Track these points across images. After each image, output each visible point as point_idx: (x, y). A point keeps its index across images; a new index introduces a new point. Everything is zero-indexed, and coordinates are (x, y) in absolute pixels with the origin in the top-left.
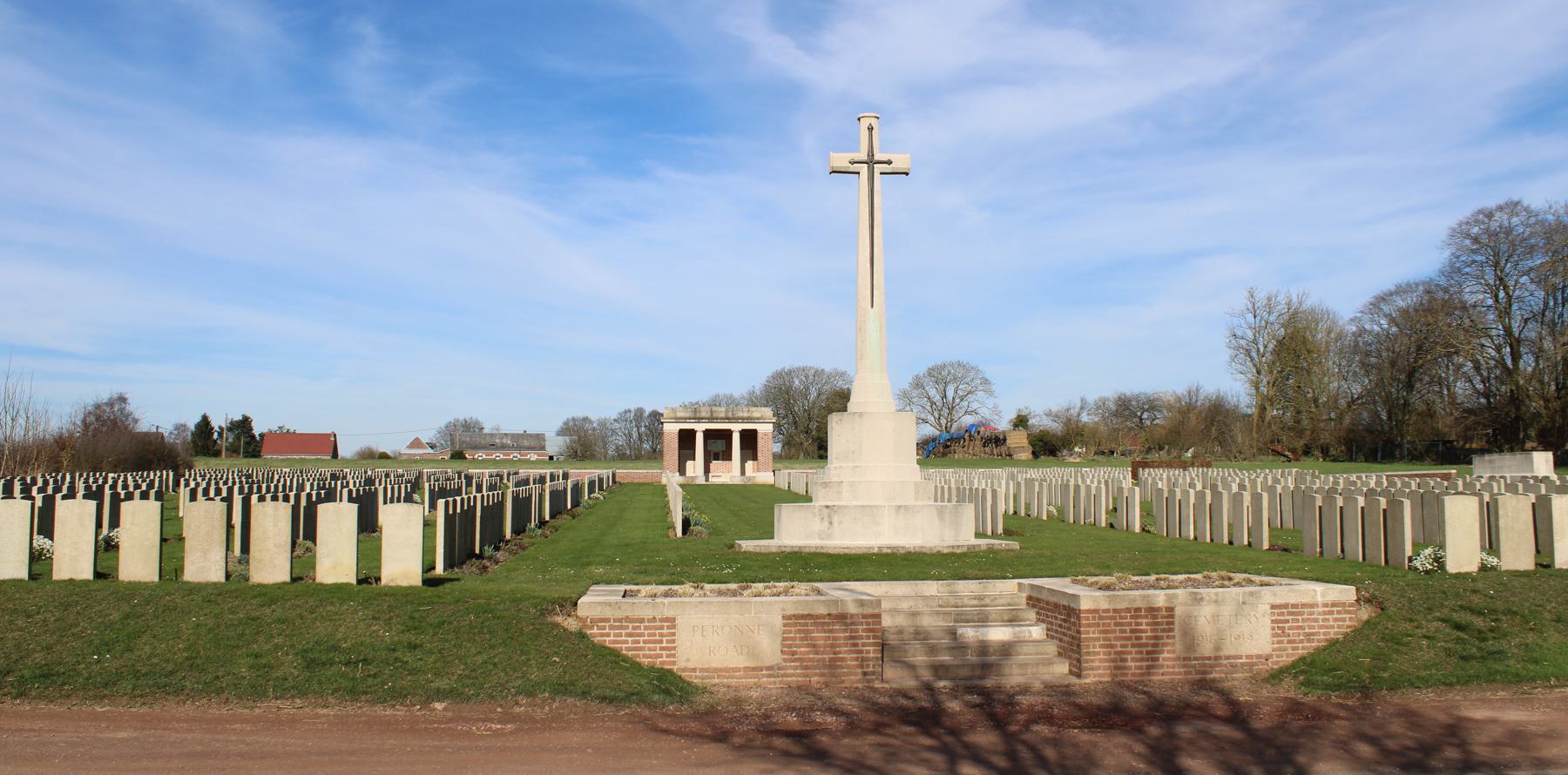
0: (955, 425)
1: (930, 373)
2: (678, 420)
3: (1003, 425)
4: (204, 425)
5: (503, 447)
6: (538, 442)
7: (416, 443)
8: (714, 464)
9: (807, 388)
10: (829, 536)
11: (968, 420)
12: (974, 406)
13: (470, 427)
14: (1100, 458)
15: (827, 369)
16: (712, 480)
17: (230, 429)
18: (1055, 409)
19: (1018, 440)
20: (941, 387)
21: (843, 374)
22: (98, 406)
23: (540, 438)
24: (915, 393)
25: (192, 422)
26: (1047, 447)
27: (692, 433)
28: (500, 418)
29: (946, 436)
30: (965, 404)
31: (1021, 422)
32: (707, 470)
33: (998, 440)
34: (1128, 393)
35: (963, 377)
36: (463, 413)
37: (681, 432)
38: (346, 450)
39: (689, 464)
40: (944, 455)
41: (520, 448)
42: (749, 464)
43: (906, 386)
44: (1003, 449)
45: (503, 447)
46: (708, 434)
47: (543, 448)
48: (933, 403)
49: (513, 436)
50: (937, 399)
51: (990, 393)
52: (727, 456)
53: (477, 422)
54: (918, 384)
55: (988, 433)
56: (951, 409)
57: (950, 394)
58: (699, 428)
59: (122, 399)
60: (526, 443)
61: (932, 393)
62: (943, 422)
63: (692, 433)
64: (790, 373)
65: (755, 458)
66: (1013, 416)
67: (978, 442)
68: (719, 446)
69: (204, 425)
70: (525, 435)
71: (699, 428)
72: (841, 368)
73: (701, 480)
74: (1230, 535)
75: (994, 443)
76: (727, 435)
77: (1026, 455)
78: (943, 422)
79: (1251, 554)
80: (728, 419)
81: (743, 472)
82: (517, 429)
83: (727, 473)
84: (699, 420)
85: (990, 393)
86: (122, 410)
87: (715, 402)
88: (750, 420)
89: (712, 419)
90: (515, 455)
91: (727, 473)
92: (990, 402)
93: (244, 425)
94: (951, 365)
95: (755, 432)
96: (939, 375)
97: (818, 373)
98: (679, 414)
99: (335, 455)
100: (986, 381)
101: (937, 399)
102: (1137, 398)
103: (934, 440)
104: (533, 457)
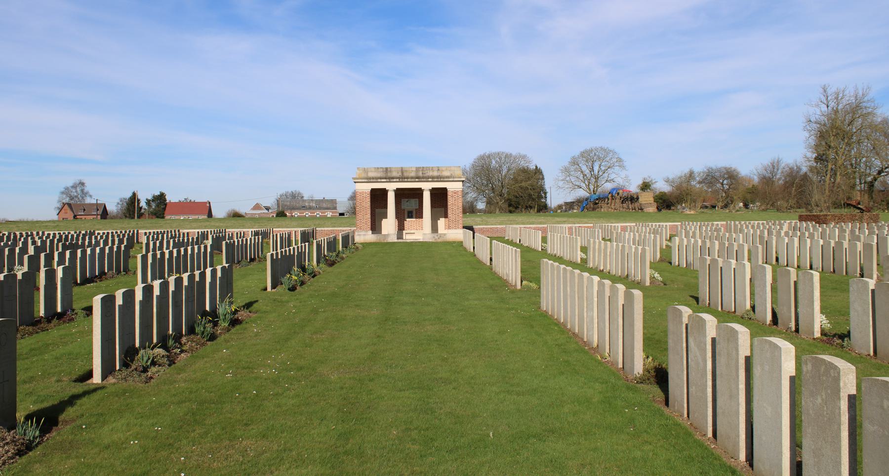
0: (599, 190)
1: (582, 154)
2: (370, 180)
3: (633, 188)
4: (133, 200)
5: (310, 208)
6: (332, 204)
7: (257, 207)
8: (409, 222)
9: (501, 167)
10: (671, 227)
11: (608, 186)
12: (612, 176)
13: (294, 196)
14: (705, 210)
15: (514, 154)
16: (408, 237)
17: (153, 201)
18: (671, 177)
19: (647, 198)
20: (590, 164)
21: (524, 157)
22: (67, 189)
23: (333, 202)
24: (572, 168)
25: (128, 195)
26: (665, 203)
27: (384, 192)
28: (313, 189)
29: (595, 197)
30: (606, 175)
31: (645, 186)
32: (401, 228)
33: (632, 199)
34: (714, 167)
35: (605, 157)
36: (290, 188)
37: (374, 192)
38: (219, 212)
39: (384, 222)
40: (594, 209)
41: (320, 208)
42: (442, 222)
43: (566, 164)
44: (636, 205)
45: (310, 208)
46: (400, 194)
47: (335, 208)
48: (585, 175)
49: (316, 201)
50: (587, 172)
51: (622, 167)
52: (419, 214)
53: (299, 193)
54: (574, 162)
55: (625, 194)
56: (597, 178)
57: (596, 168)
58: (391, 187)
59: (83, 184)
60: (325, 205)
61: (584, 168)
62: (592, 187)
63: (384, 192)
64: (489, 156)
65: (446, 216)
66: (640, 182)
67: (618, 201)
68: (412, 204)
69: (133, 200)
70: (324, 200)
71: (391, 187)
72: (523, 153)
73: (393, 239)
74: (798, 261)
75: (630, 201)
76: (418, 193)
77: (652, 209)
78: (592, 187)
79: (835, 277)
80: (419, 179)
81: (435, 228)
82: (318, 196)
83: (419, 231)
84: (390, 179)
85: (622, 167)
86: (82, 191)
87: (418, 169)
88: (440, 179)
89: (402, 179)
90: (318, 213)
91: (419, 231)
92: (623, 174)
93: (160, 199)
94: (596, 149)
95: (445, 190)
96: (589, 156)
97: (508, 156)
98: (371, 175)
99: (210, 215)
100: (620, 160)
101: (587, 172)
102: (719, 170)
103: (587, 199)
104: (329, 214)
